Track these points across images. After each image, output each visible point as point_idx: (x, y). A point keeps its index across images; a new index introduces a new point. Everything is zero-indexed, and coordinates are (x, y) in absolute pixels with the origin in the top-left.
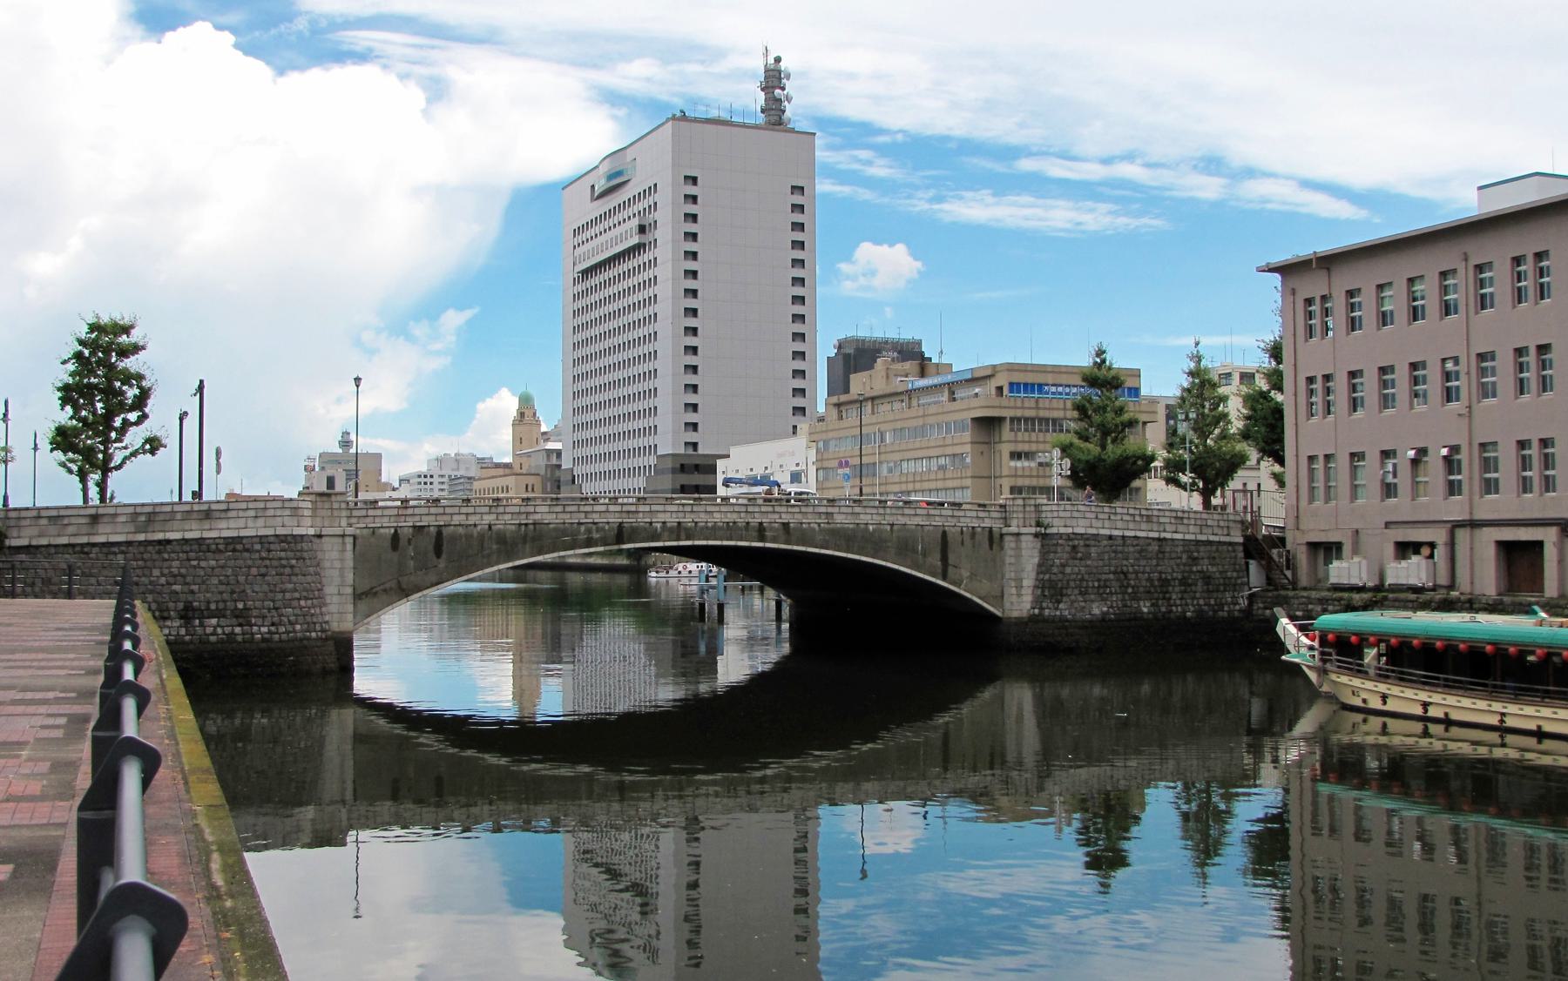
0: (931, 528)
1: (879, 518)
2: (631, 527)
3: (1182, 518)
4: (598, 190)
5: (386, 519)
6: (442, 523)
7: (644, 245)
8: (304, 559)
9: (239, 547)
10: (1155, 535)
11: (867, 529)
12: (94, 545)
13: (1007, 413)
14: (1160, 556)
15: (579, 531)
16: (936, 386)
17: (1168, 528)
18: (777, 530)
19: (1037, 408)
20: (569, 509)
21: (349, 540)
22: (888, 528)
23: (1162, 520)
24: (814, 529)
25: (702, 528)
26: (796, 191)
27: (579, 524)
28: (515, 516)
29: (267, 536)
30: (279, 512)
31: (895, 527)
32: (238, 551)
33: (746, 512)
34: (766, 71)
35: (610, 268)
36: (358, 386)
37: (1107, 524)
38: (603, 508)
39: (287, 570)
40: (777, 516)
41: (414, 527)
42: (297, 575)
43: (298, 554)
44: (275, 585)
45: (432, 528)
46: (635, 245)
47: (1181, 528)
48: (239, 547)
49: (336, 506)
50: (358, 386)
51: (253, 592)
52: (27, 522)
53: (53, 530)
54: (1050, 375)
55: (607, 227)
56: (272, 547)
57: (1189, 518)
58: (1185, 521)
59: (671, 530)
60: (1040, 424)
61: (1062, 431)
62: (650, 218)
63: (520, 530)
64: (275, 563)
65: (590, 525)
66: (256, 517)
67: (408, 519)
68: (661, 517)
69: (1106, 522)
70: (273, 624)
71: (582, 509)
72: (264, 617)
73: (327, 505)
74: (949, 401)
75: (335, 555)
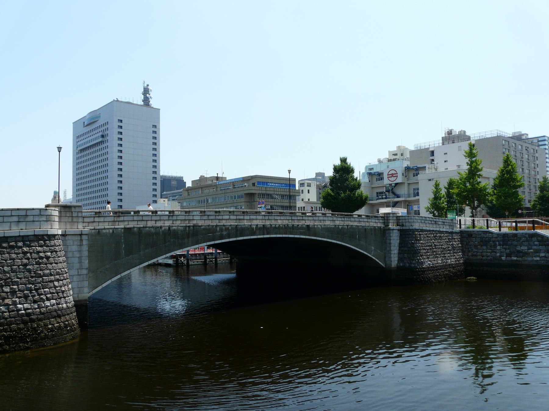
0: (361, 227)
4: (86, 124)
5: (106, 224)
6: (142, 226)
7: (104, 141)
8: (56, 252)
11: (339, 228)
13: (257, 192)
19: (266, 190)
22: (346, 227)
23: (439, 223)
24: (319, 228)
25: (300, 227)
26: (154, 127)
27: (217, 226)
29: (28, 236)
31: (349, 227)
33: (292, 219)
34: (144, 88)
35: (84, 152)
41: (125, 228)
42: (51, 264)
43: (52, 248)
45: (135, 229)
51: (18, 278)
55: (95, 133)
58: (445, 224)
60: (267, 196)
61: (273, 198)
62: (106, 133)
63: (186, 228)
65: (222, 227)
66: (19, 222)
70: (35, 302)
71: (217, 217)
72: (26, 297)
75: (485, 257)
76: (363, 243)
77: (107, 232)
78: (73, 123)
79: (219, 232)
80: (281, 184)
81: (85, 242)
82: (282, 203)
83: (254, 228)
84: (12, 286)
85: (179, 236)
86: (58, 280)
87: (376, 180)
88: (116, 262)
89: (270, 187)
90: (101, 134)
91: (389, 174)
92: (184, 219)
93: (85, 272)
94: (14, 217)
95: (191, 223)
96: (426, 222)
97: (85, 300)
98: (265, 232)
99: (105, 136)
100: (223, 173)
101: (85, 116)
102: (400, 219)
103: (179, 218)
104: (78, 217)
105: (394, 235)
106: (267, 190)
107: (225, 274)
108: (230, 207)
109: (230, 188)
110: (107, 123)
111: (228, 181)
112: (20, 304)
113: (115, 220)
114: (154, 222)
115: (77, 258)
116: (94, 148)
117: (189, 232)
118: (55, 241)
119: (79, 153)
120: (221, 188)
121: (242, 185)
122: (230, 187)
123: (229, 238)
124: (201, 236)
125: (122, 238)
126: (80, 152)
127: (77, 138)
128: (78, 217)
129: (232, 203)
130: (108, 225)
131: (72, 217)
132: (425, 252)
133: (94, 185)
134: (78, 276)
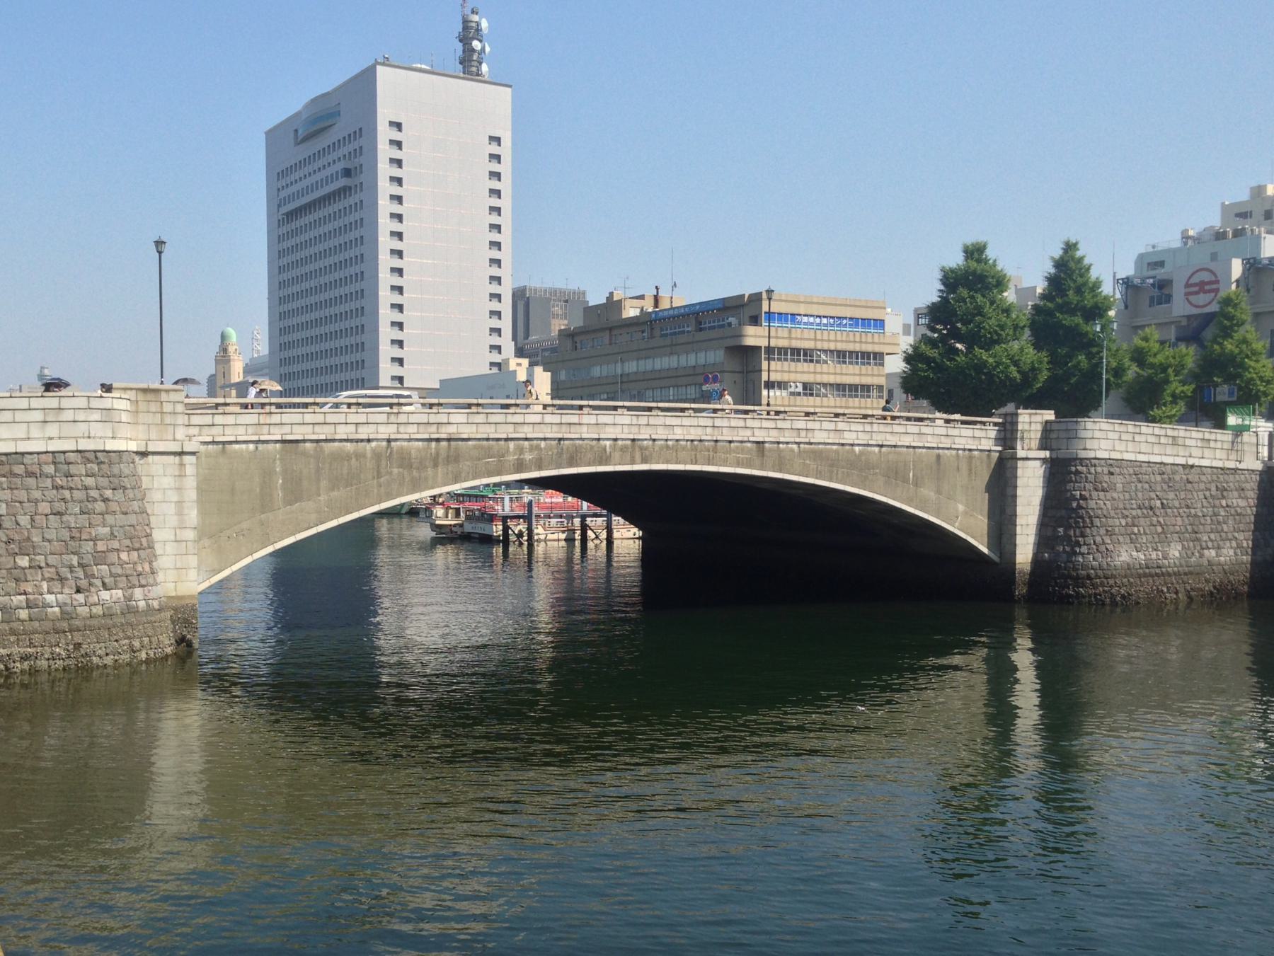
1: (867, 437)
2: (574, 445)
3: (1209, 440)
4: (300, 137)
5: (241, 430)
8: (125, 488)
9: (19, 469)
10: (1181, 461)
15: (508, 451)
16: (683, 316)
18: (750, 450)
19: (790, 338)
20: (493, 419)
23: (1188, 442)
24: (792, 450)
28: (422, 427)
30: (81, 416)
32: (16, 475)
36: (160, 253)
37: (1131, 446)
38: (537, 418)
39: (100, 506)
40: (748, 433)
43: (115, 480)
44: (80, 530)
47: (1207, 453)
48: (19, 469)
49: (168, 408)
50: (160, 253)
54: (802, 305)
56: (73, 470)
57: (1216, 441)
58: (1212, 445)
60: (792, 354)
64: (78, 495)
67: (273, 429)
68: (611, 432)
69: (1130, 444)
73: (154, 407)
74: (696, 331)
75: (167, 482)
76: (928, 492)
77: (242, 449)
79: (515, 454)
80: (839, 318)
81: (190, 470)
82: (838, 376)
83: (608, 446)
84: (33, 556)
85: (413, 461)
86: (128, 549)
87: (1150, 303)
88: (262, 516)
89: (802, 326)
90: (340, 166)
91: (1190, 283)
92: (426, 421)
93: (190, 535)
94: (34, 411)
95: (520, 430)
96: (1123, 438)
97: (192, 597)
98: (638, 456)
100: (675, 285)
102: (1053, 428)
103: (413, 418)
104: (175, 413)
105: (1029, 472)
106: (793, 336)
107: (326, 530)
108: (661, 388)
109: (689, 329)
110: (347, 138)
111: (683, 311)
112: (49, 592)
113: (262, 422)
114: (352, 428)
115: (173, 505)
116: (330, 204)
117: (438, 454)
118: (122, 465)
119: (283, 222)
120: (662, 330)
121: (712, 324)
122: (688, 327)
123: (540, 468)
124: (468, 463)
125: (278, 462)
126: (287, 217)
127: (279, 176)
128: (175, 413)
129: (690, 375)
130: (244, 432)
131: (162, 413)
132: (1124, 524)
133: (346, 312)
134: (175, 544)
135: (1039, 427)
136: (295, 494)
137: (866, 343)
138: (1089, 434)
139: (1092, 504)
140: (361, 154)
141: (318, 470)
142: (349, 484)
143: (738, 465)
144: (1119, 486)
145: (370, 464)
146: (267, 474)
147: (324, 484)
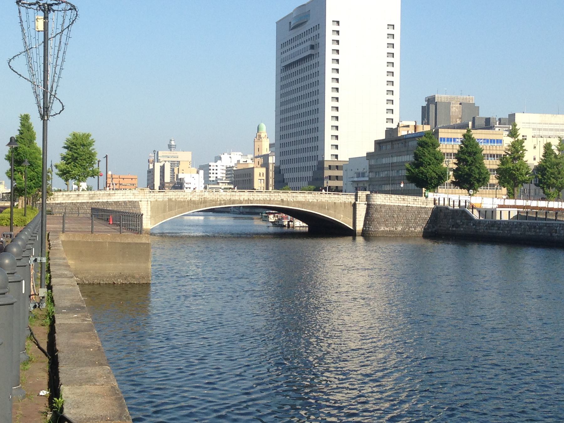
12: (78, 203)
14: (407, 212)
17: (411, 202)
18: (279, 201)
21: (149, 202)
30: (129, 194)
46: (302, 58)
47: (415, 203)
49: (145, 192)
52: (60, 196)
53: (67, 198)
59: (246, 201)
75: (145, 207)
76: (331, 212)
78: (276, 23)
90: (309, 43)
93: (149, 217)
99: (315, 46)
101: (292, 13)
123: (225, 205)
135: (365, 196)
136: (170, 209)
137: (493, 150)
138: (375, 198)
139: (374, 215)
140: (319, 38)
141: (176, 205)
142: (181, 208)
143: (276, 204)
144: (383, 211)
145: (186, 204)
146: (165, 205)
147: (177, 207)
